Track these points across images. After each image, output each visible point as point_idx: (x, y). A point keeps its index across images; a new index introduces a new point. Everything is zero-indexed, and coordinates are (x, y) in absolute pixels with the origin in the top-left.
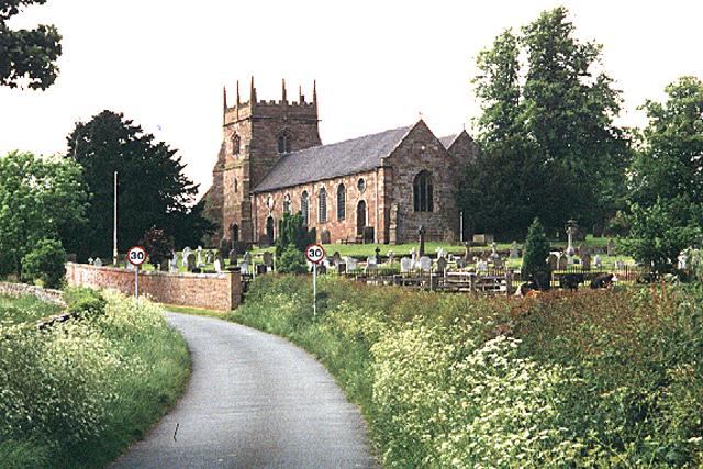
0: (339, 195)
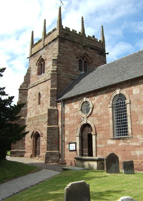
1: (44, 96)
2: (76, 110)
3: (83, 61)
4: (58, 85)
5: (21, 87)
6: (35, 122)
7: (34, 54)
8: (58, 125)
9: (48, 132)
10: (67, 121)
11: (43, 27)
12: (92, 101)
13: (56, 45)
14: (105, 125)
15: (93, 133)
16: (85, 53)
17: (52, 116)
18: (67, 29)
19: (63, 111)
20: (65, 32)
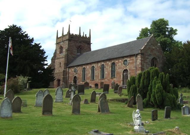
0: (112, 67)
1: (62, 64)
2: (73, 71)
3: (79, 48)
6: (58, 75)
7: (58, 43)
8: (67, 76)
9: (63, 79)
10: (70, 75)
11: (62, 31)
14: (80, 77)
16: (80, 45)
18: (73, 34)
19: (69, 71)
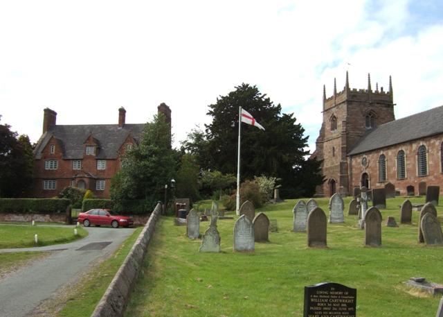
4: (347, 143)
5: (317, 140)
10: (354, 171)
12: (369, 157)
13: (345, 106)
15: (369, 179)
16: (372, 110)
17: (343, 167)
18: (355, 90)
19: (351, 164)
20: (353, 94)
